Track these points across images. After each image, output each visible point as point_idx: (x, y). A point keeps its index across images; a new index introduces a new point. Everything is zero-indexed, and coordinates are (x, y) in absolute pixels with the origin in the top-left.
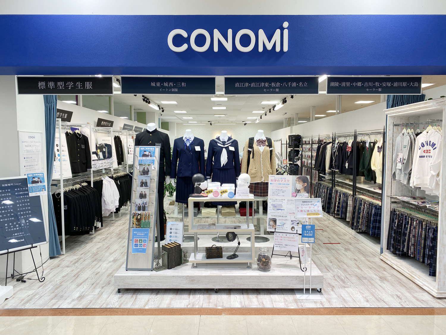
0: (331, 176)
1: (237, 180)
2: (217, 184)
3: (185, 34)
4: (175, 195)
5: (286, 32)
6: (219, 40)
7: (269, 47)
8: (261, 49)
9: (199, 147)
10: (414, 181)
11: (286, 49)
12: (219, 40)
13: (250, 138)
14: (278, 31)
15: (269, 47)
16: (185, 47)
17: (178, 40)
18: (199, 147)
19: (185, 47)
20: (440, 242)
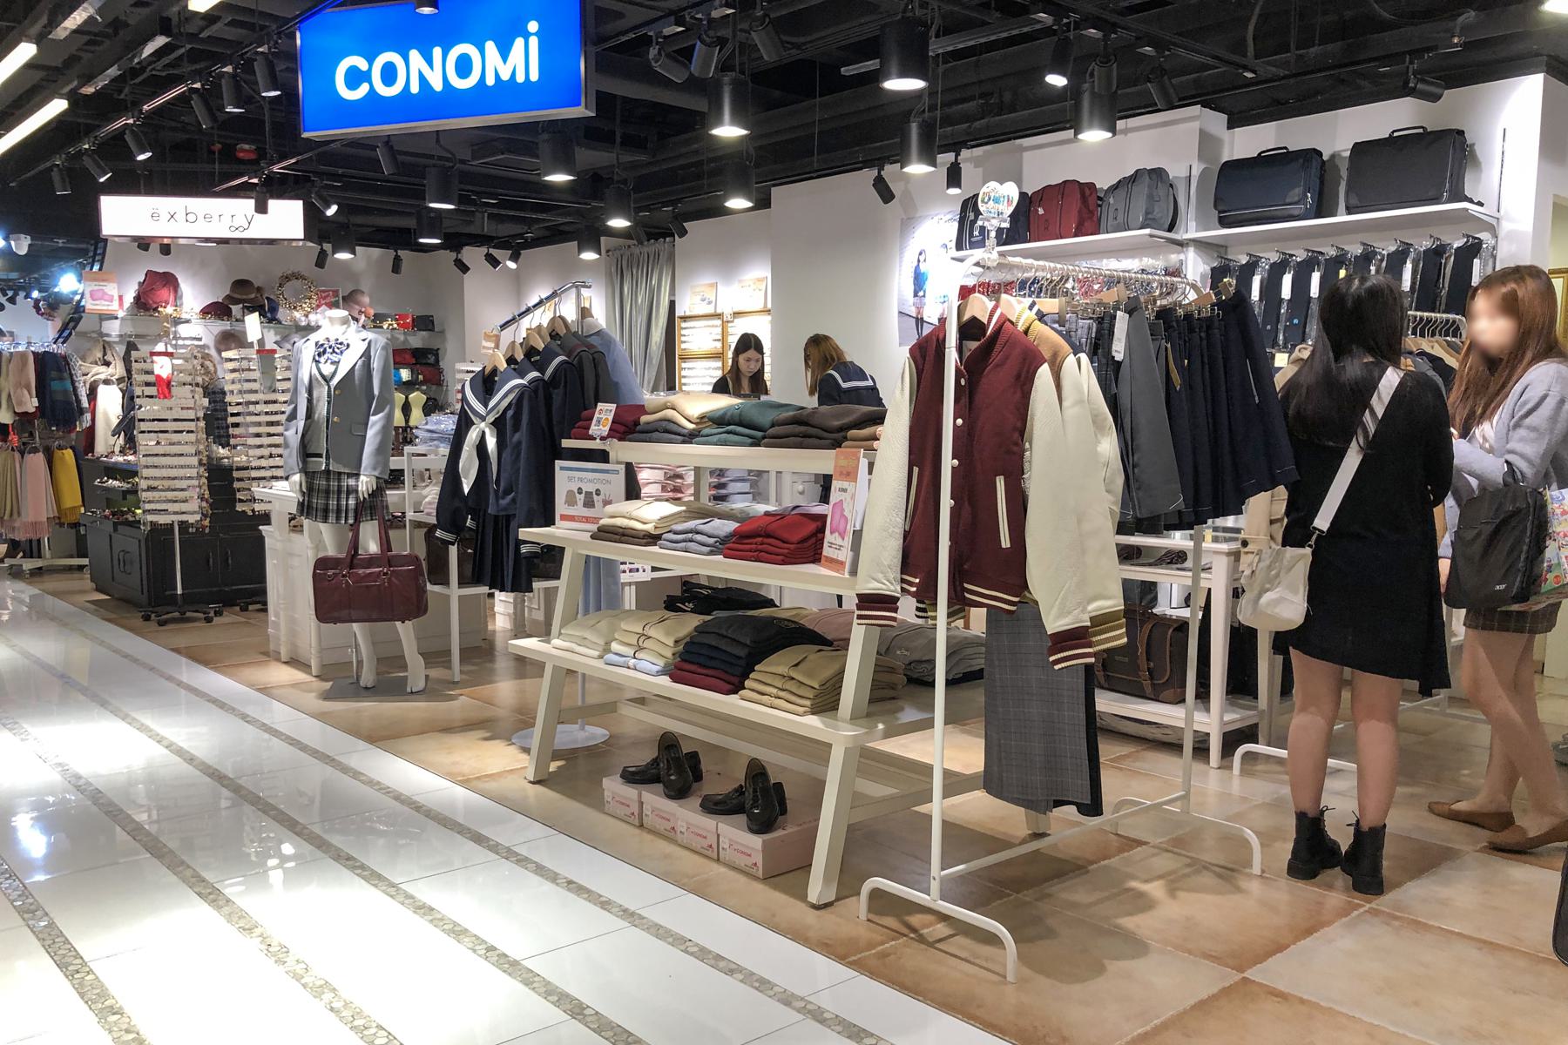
0: (1533, 458)
1: (1414, 685)
2: (898, 392)
3: (362, 64)
4: (1130, 261)
5: (534, 41)
6: (420, 73)
7: (505, 76)
8: (490, 81)
9: (301, 202)
10: (870, 472)
11: (534, 77)
12: (420, 73)
13: (425, 611)
14: (519, 42)
15: (505, 76)
16: (363, 90)
17: (355, 76)
18: (301, 202)
19: (363, 90)
20: (724, 571)
